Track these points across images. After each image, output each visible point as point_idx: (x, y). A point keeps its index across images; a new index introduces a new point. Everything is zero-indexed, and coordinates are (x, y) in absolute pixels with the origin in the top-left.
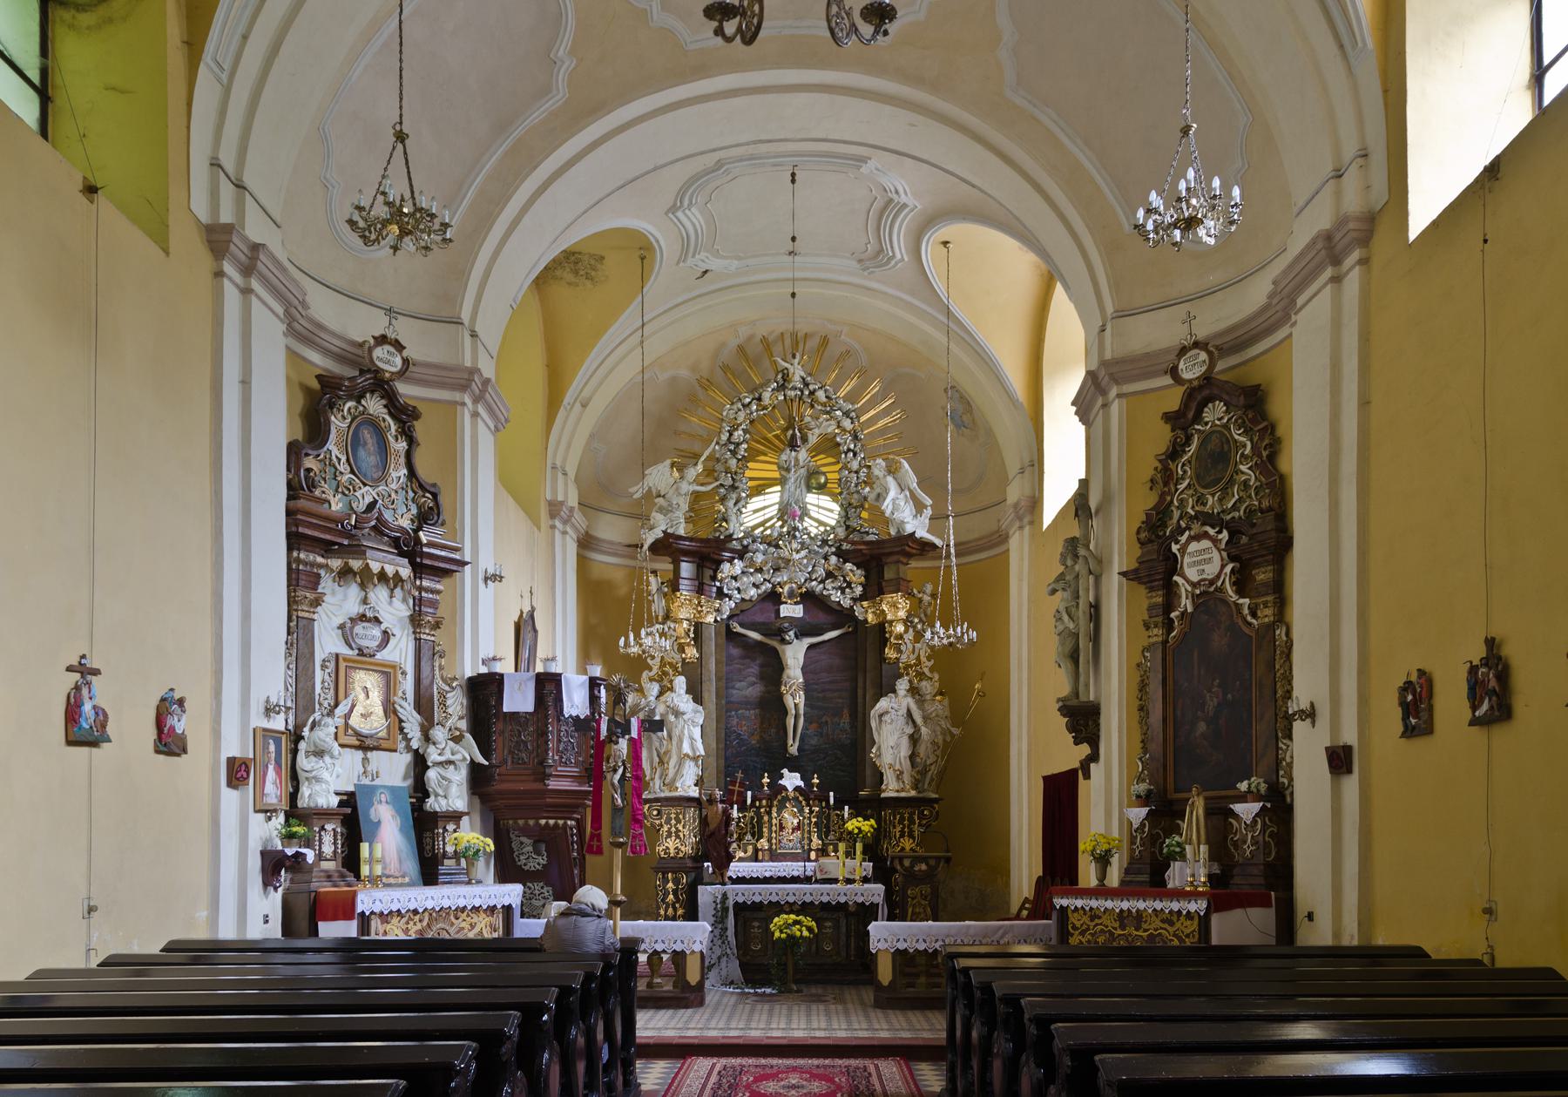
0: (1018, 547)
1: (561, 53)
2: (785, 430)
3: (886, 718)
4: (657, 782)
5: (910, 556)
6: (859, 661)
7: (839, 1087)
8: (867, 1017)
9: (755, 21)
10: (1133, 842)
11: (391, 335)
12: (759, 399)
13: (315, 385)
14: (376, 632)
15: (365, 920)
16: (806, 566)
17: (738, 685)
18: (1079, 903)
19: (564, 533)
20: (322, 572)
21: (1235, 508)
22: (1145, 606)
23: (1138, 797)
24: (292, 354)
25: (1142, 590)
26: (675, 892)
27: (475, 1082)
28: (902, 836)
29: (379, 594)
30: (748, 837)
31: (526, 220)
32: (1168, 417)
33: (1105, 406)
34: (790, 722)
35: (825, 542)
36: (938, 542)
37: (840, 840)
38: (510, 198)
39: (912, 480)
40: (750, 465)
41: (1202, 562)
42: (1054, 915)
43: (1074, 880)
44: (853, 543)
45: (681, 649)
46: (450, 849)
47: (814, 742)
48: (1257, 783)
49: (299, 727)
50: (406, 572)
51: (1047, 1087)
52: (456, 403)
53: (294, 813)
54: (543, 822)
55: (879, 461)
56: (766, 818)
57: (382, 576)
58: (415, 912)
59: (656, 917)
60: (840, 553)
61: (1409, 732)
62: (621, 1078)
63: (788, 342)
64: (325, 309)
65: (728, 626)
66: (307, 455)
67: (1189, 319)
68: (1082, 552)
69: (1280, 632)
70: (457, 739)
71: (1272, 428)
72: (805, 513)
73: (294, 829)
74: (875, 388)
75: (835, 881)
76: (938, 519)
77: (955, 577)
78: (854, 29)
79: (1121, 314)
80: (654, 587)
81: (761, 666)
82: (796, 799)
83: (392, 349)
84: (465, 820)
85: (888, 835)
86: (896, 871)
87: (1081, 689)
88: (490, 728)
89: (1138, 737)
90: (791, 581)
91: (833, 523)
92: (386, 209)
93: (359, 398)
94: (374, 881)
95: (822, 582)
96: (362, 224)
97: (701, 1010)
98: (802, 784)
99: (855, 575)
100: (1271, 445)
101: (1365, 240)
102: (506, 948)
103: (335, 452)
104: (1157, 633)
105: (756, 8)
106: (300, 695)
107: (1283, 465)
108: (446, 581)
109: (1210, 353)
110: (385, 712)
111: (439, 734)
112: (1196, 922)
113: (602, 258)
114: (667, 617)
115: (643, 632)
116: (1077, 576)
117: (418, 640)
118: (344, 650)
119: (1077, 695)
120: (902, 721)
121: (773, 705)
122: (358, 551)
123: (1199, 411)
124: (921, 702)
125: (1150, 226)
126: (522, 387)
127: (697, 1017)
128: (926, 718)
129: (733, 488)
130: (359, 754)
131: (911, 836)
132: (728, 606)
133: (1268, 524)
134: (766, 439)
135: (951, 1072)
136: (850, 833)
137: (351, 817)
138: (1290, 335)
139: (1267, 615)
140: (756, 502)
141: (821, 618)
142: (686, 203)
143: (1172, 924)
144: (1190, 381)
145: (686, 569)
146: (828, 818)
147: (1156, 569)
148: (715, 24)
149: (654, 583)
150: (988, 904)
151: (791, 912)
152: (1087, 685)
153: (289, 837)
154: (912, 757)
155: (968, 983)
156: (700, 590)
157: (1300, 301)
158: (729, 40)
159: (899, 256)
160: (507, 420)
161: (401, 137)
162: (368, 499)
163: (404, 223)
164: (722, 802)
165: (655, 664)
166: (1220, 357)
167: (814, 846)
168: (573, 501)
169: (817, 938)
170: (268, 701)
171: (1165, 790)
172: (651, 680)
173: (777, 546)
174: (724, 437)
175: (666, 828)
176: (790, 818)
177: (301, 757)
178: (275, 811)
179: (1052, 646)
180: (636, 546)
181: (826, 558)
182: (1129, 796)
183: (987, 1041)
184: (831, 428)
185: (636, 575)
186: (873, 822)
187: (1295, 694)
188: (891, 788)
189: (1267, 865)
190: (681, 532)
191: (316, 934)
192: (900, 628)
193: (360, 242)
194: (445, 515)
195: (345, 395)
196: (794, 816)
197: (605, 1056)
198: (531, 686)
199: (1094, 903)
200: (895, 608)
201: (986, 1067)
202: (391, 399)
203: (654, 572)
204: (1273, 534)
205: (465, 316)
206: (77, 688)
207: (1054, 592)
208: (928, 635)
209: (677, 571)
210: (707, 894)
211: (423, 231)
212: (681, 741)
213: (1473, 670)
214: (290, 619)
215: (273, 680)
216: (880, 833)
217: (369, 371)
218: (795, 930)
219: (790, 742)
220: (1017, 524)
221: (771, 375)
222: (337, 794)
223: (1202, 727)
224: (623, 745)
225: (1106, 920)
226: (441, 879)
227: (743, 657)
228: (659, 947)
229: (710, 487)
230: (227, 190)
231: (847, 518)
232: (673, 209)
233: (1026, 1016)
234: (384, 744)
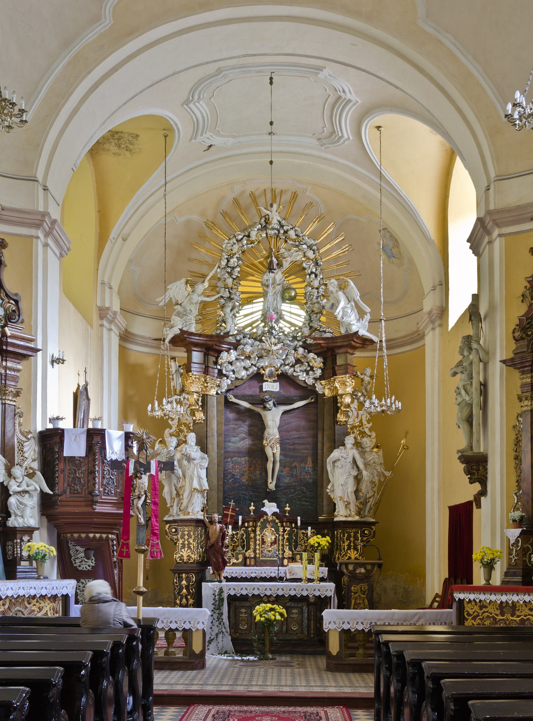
5: (355, 348)
6: (321, 420)
17: (233, 439)
25: (516, 374)
35: (295, 338)
44: (315, 339)
45: (193, 413)
47: (287, 480)
60: (305, 346)
63: (269, 196)
68: (474, 346)
72: (281, 317)
74: (330, 229)
77: (386, 363)
81: (250, 426)
89: (514, 478)
90: (270, 365)
99: (317, 362)
108: (24, 362)
111: (17, 471)
114: (183, 391)
124: (363, 453)
129: (230, 299)
131: (355, 549)
132: (226, 383)
140: (247, 309)
141: (292, 392)
145: (197, 356)
152: (478, 441)
154: (357, 492)
156: (206, 371)
165: (174, 424)
168: (116, 307)
173: (261, 341)
174: (224, 263)
181: (295, 349)
184: (299, 257)
186: (328, 538)
188: (342, 514)
190: (193, 330)
192: (347, 400)
200: (344, 386)
205: (40, 176)
212: (192, 479)
219: (270, 480)
231: (311, 320)
232: (187, 102)
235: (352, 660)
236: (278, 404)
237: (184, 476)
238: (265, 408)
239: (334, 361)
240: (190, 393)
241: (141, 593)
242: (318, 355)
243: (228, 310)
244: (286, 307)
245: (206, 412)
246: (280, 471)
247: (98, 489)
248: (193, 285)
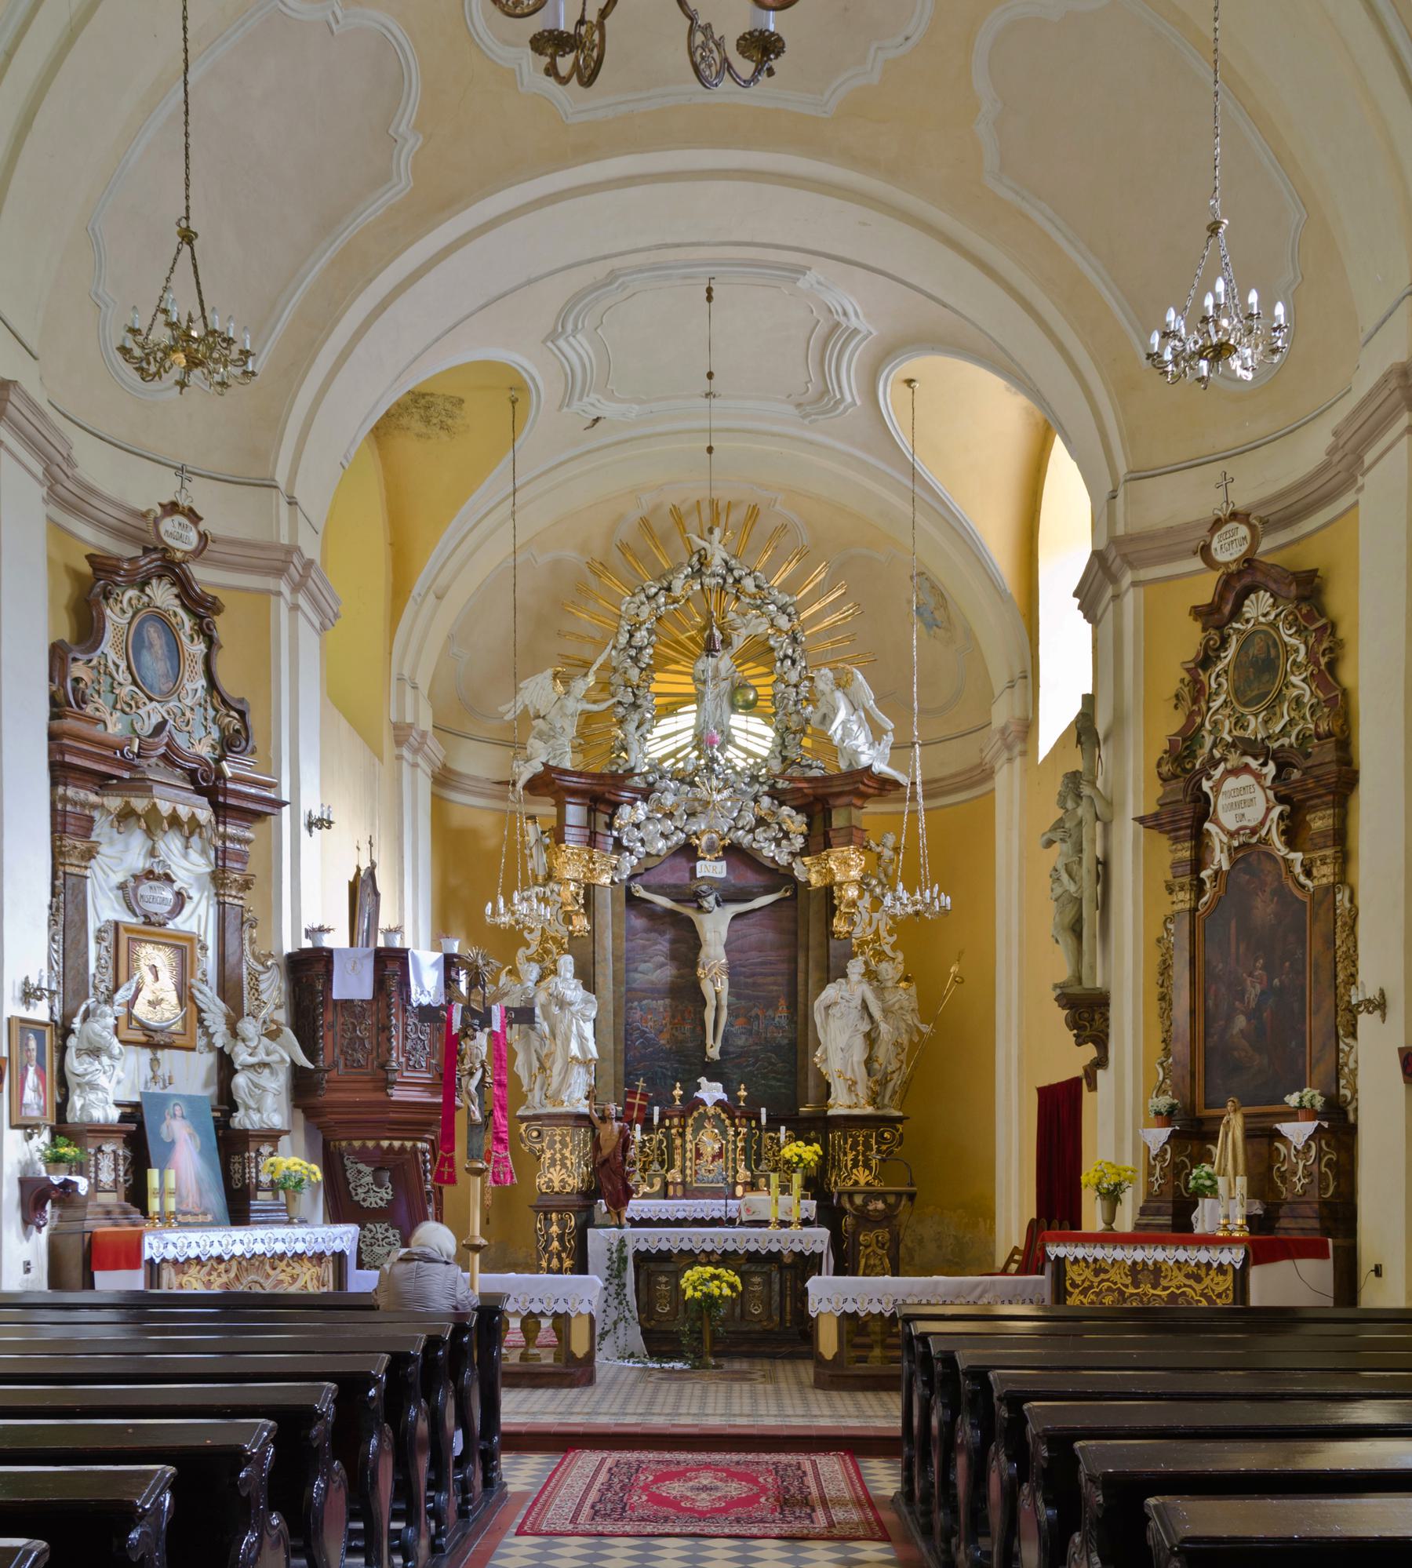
0: (1007, 783)
1: (402, 128)
2: (704, 629)
5: (865, 796)
6: (801, 932)
7: (764, 1490)
8: (804, 1399)
9: (595, 54)
10: (1150, 1174)
11: (184, 502)
12: (669, 589)
13: (86, 568)
14: (168, 894)
15: (154, 1269)
16: (730, 811)
17: (643, 967)
18: (1080, 1252)
19: (415, 765)
20: (96, 814)
21: (1284, 732)
22: (1168, 863)
23: (1158, 1113)
24: (54, 525)
25: (1164, 842)
26: (561, 1238)
27: (272, 1473)
28: (855, 1165)
29: (171, 845)
30: (656, 1166)
31: (359, 350)
32: (1198, 612)
34: (709, 1015)
35: (754, 778)
37: (774, 1170)
38: (338, 320)
39: (868, 697)
40: (657, 676)
41: (1242, 803)
42: (1048, 1268)
43: (1076, 1223)
44: (791, 780)
45: (568, 919)
46: (265, 1178)
48: (1312, 1096)
49: (67, 1017)
50: (205, 814)
51: (1021, 1485)
52: (269, 592)
53: (62, 1128)
54: (385, 1144)
55: (825, 671)
56: (678, 1142)
57: (175, 821)
58: (219, 1259)
59: (538, 1269)
60: (774, 794)
62: (479, 1476)
63: (706, 512)
64: (95, 465)
65: (628, 889)
66: (75, 660)
67: (1226, 481)
68: (1086, 790)
69: (1342, 897)
70: (273, 1035)
71: (1332, 627)
72: (728, 740)
73: (63, 1150)
74: (819, 574)
75: (765, 1223)
76: (901, 747)
77: (922, 824)
78: (727, 66)
79: (1137, 476)
80: (531, 838)
81: (673, 942)
82: (717, 1116)
83: (185, 521)
84: (285, 1141)
85: (837, 1165)
86: (844, 1212)
87: (1085, 971)
88: (315, 1020)
89: (1158, 1036)
91: (765, 753)
92: (168, 331)
93: (143, 585)
94: (165, 1218)
95: (751, 831)
96: (137, 352)
97: (590, 1390)
98: (724, 1097)
99: (796, 823)
100: (1331, 650)
102: (338, 1304)
104: (1184, 898)
105: (596, 37)
106: (69, 976)
107: (1346, 676)
108: (258, 826)
109: (1252, 527)
110: (180, 998)
112: (1230, 1277)
113: (461, 401)
114: (549, 877)
115: (516, 897)
116: (1080, 822)
117: (221, 904)
118: (127, 918)
119: (1080, 980)
120: (855, 1014)
121: (686, 993)
122: (141, 786)
124: (880, 990)
125: (1168, 356)
126: (357, 572)
127: (585, 1398)
128: (886, 1011)
129: (635, 706)
130: (146, 1054)
131: (867, 1166)
132: (629, 863)
133: (1326, 753)
134: (678, 642)
135: (908, 1468)
136: (788, 1162)
138: (1356, 504)
139: (1325, 874)
140: (667, 725)
141: (751, 879)
142: (570, 327)
143: (1198, 1279)
144: (1226, 564)
145: (575, 813)
146: (759, 1142)
147: (1185, 815)
148: (547, 60)
149: (532, 832)
150: (964, 1256)
151: (709, 1263)
152: (1093, 968)
153: (56, 1160)
154: (869, 1062)
155: (927, 1353)
156: (592, 841)
157: (1368, 458)
158: (563, 81)
159: (848, 399)
160: (337, 616)
161: (187, 237)
162: (156, 719)
163: (199, 350)
164: (618, 1119)
165: (534, 939)
166: (1266, 533)
168: (426, 723)
169: (742, 1298)
170: (26, 982)
171: (1193, 1102)
172: (529, 959)
173: (692, 784)
174: (623, 639)
175: (548, 1154)
176: (709, 1141)
177: (71, 1054)
178: (37, 1126)
179: (1048, 917)
180: (507, 783)
181: (756, 800)
182: (1146, 1114)
183: (949, 1427)
184: (762, 627)
185: (508, 819)
186: (817, 1147)
187: (1360, 978)
188: (841, 1104)
189: (1324, 1203)
190: (567, 764)
191: (92, 1286)
192: (852, 892)
193: (136, 376)
194: (256, 740)
195: (127, 582)
196: (715, 1139)
197: (458, 1445)
198: (369, 966)
199: (1099, 1252)
200: (846, 867)
201: (947, 1465)
203: (532, 818)
204: (1334, 767)
205: (281, 479)
207: (1050, 843)
208: (888, 900)
209: (561, 816)
210: (599, 1240)
211: (216, 361)
214: (54, 876)
216: (826, 1162)
217: (155, 549)
218: (713, 1288)
219: (709, 1041)
220: (1005, 755)
221: (684, 557)
222: (118, 1105)
223: (1241, 1022)
224: (482, 1040)
225: (1113, 1275)
226: (254, 1217)
227: (648, 930)
228: (536, 1308)
229: (603, 706)
231: (784, 746)
232: (553, 336)
233: (996, 1394)
234: (179, 1041)
235: (860, 1368)
236: (725, 899)
238: (700, 908)
241: (477, 1248)
242: (798, 809)
244: (737, 720)
245: (592, 919)
246: (729, 1024)
247: (396, 1059)
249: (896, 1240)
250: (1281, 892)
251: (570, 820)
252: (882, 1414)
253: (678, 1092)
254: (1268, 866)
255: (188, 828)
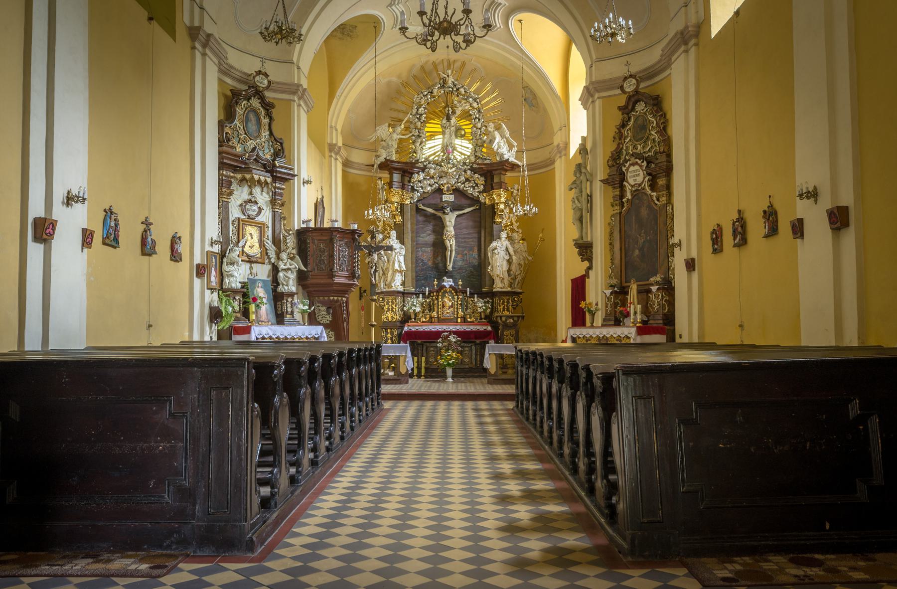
2: (445, 107)
3: (496, 251)
4: (382, 284)
5: (506, 171)
6: (483, 221)
11: (263, 71)
13: (229, 94)
14: (255, 208)
17: (422, 235)
24: (220, 81)
25: (610, 188)
29: (257, 190)
30: (427, 311)
32: (620, 108)
33: (593, 102)
35: (464, 164)
36: (519, 163)
41: (636, 176)
44: (478, 164)
45: (394, 217)
47: (460, 263)
50: (269, 180)
57: (259, 181)
60: (472, 169)
61: (715, 251)
63: (445, 64)
67: (628, 64)
68: (583, 170)
70: (292, 259)
71: (664, 115)
72: (454, 149)
74: (489, 87)
77: (527, 182)
81: (434, 226)
82: (450, 292)
85: (496, 310)
89: (609, 257)
90: (448, 183)
99: (481, 180)
101: (697, 35)
103: (238, 124)
104: (617, 209)
108: (287, 183)
109: (637, 80)
111: (284, 256)
114: (386, 201)
118: (242, 217)
121: (439, 246)
122: (248, 170)
123: (634, 107)
124: (512, 244)
128: (515, 252)
129: (419, 136)
130: (248, 265)
131: (508, 310)
132: (417, 195)
133: (662, 158)
137: (245, 294)
139: (664, 200)
140: (430, 144)
141: (464, 202)
145: (397, 177)
147: (617, 179)
149: (380, 184)
152: (587, 233)
154: (509, 271)
156: (403, 188)
157: (673, 59)
162: (252, 146)
165: (381, 224)
167: (459, 315)
168: (340, 144)
173: (441, 166)
174: (414, 111)
177: (225, 264)
181: (465, 171)
184: (468, 107)
188: (498, 286)
189: (664, 315)
190: (394, 159)
192: (502, 206)
194: (286, 153)
200: (500, 197)
202: (262, 99)
205: (295, 60)
206: (145, 231)
207: (571, 189)
212: (394, 263)
213: (734, 224)
215: (213, 231)
230: (197, 10)
231: (476, 151)
232: (390, 5)
235: (504, 377)
236: (454, 209)
237: (388, 261)
238: (444, 213)
239: (492, 179)
240: (392, 203)
241: (373, 326)
242: (481, 175)
243: (418, 144)
244: (457, 142)
245: (403, 217)
246: (455, 257)
247: (336, 267)
248: (393, 127)
249: (517, 333)
250: (650, 208)
251: (395, 180)
252: (511, 389)
253: (436, 283)
254: (645, 197)
255: (262, 184)
